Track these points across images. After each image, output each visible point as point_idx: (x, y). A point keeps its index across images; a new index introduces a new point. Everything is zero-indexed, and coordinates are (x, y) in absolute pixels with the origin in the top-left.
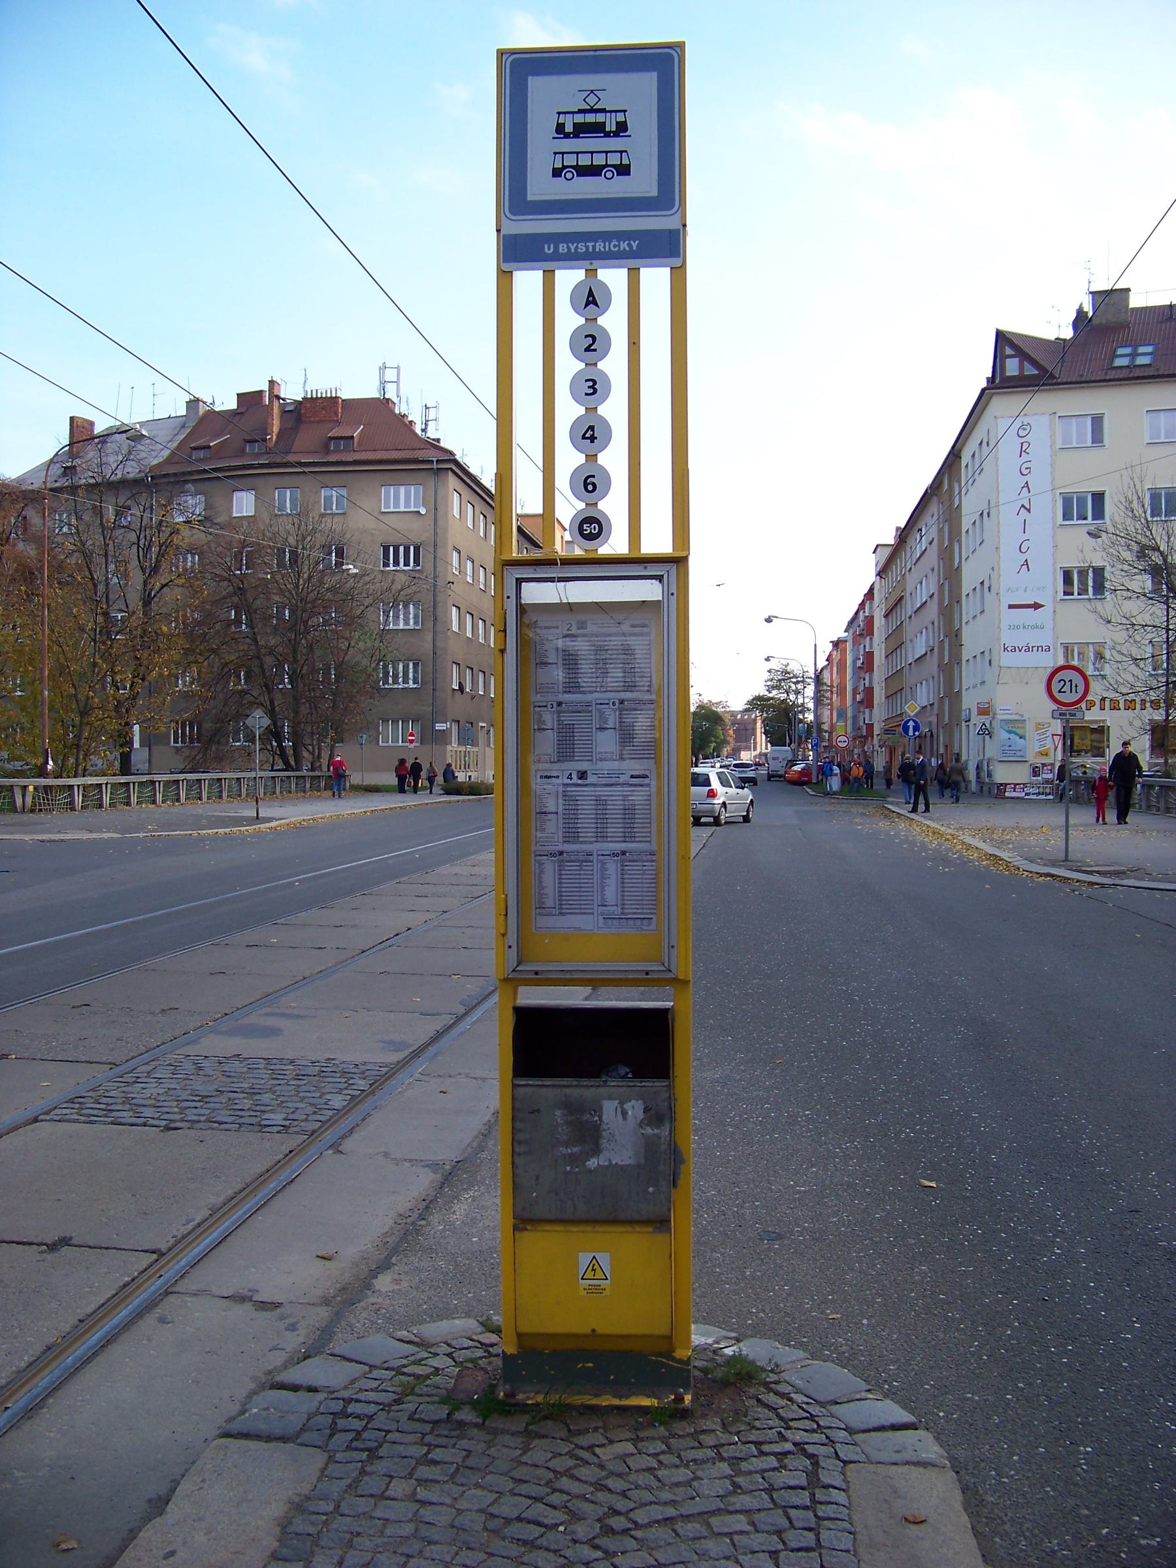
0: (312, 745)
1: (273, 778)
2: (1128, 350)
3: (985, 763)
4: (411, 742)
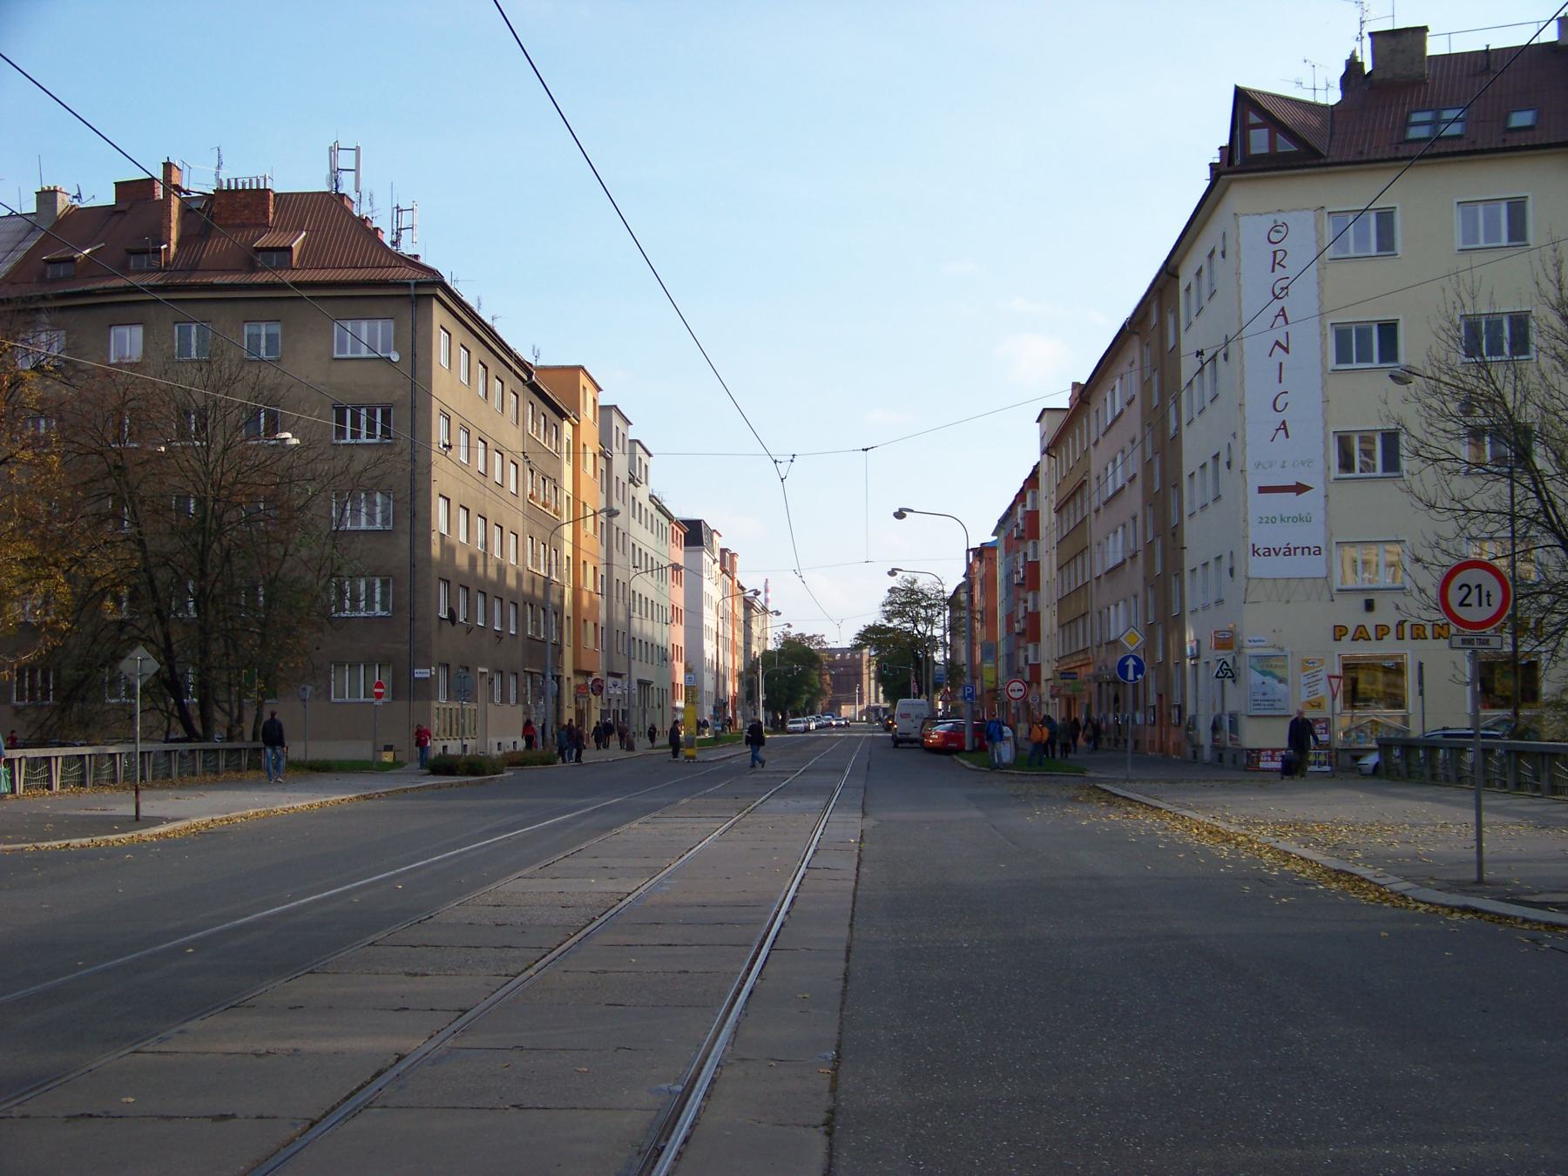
0: (230, 702)
1: (168, 753)
2: (1427, 116)
3: (1226, 720)
4: (379, 696)
